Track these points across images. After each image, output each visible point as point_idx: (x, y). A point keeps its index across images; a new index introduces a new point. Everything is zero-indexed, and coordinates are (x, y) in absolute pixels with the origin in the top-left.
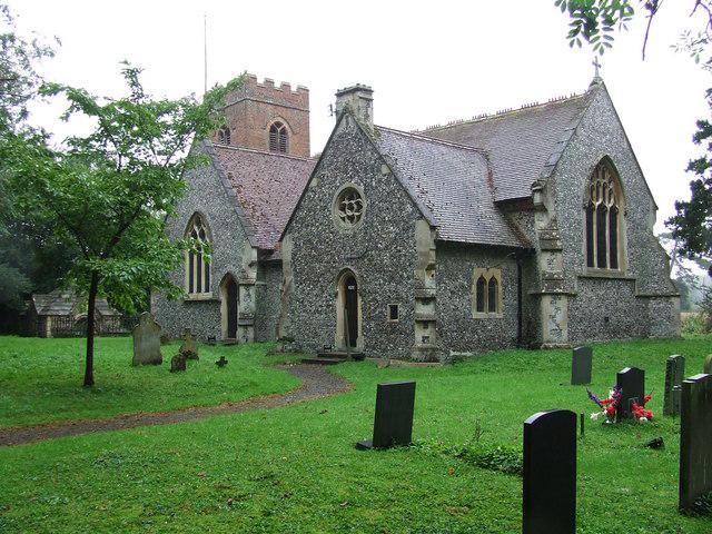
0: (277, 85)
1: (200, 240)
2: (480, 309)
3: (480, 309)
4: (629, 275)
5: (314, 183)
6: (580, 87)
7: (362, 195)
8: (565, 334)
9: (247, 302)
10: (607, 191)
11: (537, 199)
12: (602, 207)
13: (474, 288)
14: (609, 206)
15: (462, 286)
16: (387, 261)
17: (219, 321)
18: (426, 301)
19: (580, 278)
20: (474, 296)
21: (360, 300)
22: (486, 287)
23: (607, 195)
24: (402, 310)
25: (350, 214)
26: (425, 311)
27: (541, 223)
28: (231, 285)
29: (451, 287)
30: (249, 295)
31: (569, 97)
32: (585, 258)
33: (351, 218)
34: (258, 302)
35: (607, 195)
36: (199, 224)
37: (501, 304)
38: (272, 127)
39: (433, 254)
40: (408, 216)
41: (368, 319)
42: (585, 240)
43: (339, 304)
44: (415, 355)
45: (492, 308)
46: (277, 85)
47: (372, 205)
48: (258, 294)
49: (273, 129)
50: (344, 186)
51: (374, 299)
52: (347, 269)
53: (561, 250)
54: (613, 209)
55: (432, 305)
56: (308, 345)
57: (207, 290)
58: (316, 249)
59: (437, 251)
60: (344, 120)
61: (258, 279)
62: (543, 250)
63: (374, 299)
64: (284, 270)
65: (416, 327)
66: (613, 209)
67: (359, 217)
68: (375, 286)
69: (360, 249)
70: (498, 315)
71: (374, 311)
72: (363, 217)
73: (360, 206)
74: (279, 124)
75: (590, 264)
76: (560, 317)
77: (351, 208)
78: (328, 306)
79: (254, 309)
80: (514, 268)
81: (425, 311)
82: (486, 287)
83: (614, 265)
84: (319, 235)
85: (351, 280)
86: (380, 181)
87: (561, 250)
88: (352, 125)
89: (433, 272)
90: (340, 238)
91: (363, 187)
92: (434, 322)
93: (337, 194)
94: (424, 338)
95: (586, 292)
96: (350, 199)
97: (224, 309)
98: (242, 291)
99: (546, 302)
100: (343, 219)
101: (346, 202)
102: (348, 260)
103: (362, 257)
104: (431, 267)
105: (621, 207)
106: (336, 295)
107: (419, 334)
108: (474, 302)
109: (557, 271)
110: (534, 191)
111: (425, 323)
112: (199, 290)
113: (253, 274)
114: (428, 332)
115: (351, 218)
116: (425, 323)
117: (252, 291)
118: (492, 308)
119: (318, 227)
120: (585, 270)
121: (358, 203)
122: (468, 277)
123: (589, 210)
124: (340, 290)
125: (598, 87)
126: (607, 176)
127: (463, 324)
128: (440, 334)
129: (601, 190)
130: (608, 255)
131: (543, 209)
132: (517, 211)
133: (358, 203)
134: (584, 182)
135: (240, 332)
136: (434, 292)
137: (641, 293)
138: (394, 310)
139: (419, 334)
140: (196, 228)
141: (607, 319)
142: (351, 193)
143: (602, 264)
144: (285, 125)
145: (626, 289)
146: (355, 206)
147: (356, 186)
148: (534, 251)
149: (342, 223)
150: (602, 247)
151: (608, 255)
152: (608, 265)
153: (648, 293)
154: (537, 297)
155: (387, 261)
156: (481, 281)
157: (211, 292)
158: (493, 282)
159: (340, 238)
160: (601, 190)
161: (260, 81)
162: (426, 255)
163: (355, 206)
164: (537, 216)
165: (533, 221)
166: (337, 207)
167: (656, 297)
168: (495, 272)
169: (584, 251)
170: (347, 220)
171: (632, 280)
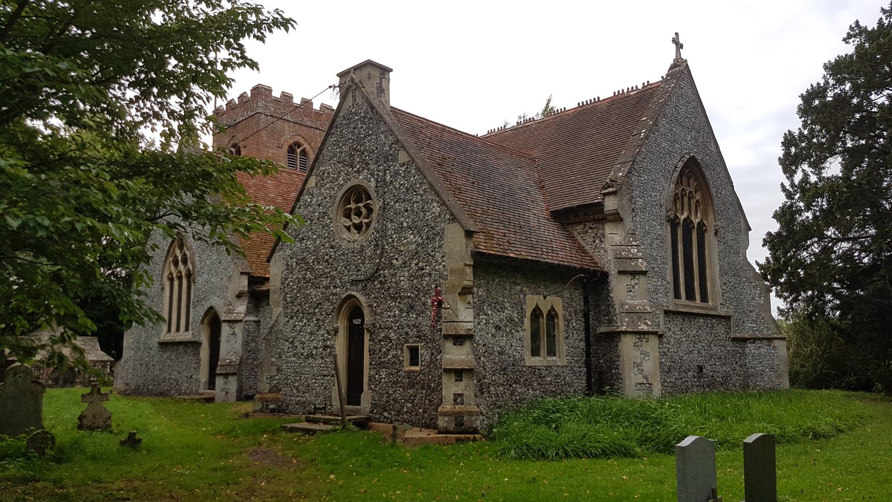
0: (297, 100)
1: (181, 266)
2: (535, 352)
3: (535, 352)
4: (722, 312)
5: (312, 181)
6: (654, 70)
7: (373, 195)
8: (657, 390)
9: (231, 346)
10: (693, 201)
11: (610, 204)
12: (688, 222)
13: (527, 321)
14: (696, 221)
15: (511, 320)
16: (405, 284)
17: (197, 369)
18: (459, 339)
19: (667, 313)
20: (527, 334)
21: (367, 337)
22: (543, 322)
23: (693, 207)
24: (424, 354)
25: (356, 220)
26: (457, 355)
27: (614, 235)
28: (213, 322)
29: (496, 319)
30: (234, 334)
31: (640, 87)
32: (671, 287)
33: (358, 227)
34: (246, 343)
35: (693, 207)
36: (181, 247)
37: (562, 345)
38: (290, 147)
39: (469, 270)
40: (435, 218)
41: (378, 365)
42: (670, 263)
43: (340, 345)
44: (442, 422)
45: (551, 352)
46: (297, 100)
47: (384, 208)
48: (247, 332)
49: (291, 150)
50: (349, 185)
51: (387, 337)
52: (351, 296)
53: (644, 273)
54: (701, 225)
55: (467, 347)
56: (298, 403)
57: (187, 329)
58: (312, 270)
59: (475, 267)
60: (350, 96)
61: (248, 312)
62: (620, 273)
63: (387, 337)
64: (271, 302)
65: (444, 374)
66: (701, 225)
67: (368, 225)
68: (384, 316)
69: (367, 268)
70: (560, 360)
71: (386, 354)
72: (374, 225)
73: (370, 210)
74: (298, 145)
75: (677, 295)
76: (650, 365)
77: (359, 214)
78: (326, 347)
79: (240, 351)
80: (578, 296)
81: (457, 355)
82: (543, 322)
83: (704, 299)
84: (317, 250)
85: (356, 311)
86: (397, 173)
87: (644, 273)
88: (359, 100)
89: (469, 297)
90: (343, 254)
91: (373, 184)
92: (470, 371)
93: (340, 195)
94: (457, 396)
95: (675, 330)
96: (357, 201)
97: (204, 352)
98: (225, 329)
99: (627, 345)
100: (348, 228)
101: (353, 206)
102: (354, 282)
103: (371, 278)
104: (466, 291)
105: (710, 224)
106: (336, 331)
107: (450, 388)
108: (528, 342)
109: (640, 302)
110: (605, 195)
111: (459, 374)
112: (178, 330)
113: (241, 308)
114: (460, 387)
115: (358, 227)
116: (459, 374)
117: (238, 328)
118: (551, 352)
119: (315, 240)
120: (670, 303)
121: (367, 207)
122: (519, 306)
123: (673, 223)
124: (342, 325)
125: (680, 72)
126: (693, 184)
127: (514, 373)
128: (481, 390)
129: (686, 200)
130: (696, 284)
131: (616, 218)
132: (581, 223)
133: (367, 207)
134: (670, 188)
135: (219, 381)
136: (470, 326)
137: (738, 335)
138: (414, 351)
139: (450, 388)
140: (178, 252)
141: (700, 369)
142: (358, 193)
143: (690, 296)
144: (306, 145)
145: (720, 329)
146: (364, 210)
147: (364, 183)
148: (605, 276)
149: (347, 233)
150: (690, 276)
151: (696, 284)
152: (698, 297)
153: (747, 336)
154: (614, 337)
155: (405, 284)
156: (536, 314)
157: (190, 332)
158: (552, 315)
159: (343, 254)
160: (686, 200)
161: (276, 94)
162: (461, 273)
163: (364, 210)
164: (609, 229)
165: (603, 235)
166: (341, 213)
167: (755, 339)
168: (553, 301)
169: (670, 277)
170: (352, 229)
171: (728, 318)
